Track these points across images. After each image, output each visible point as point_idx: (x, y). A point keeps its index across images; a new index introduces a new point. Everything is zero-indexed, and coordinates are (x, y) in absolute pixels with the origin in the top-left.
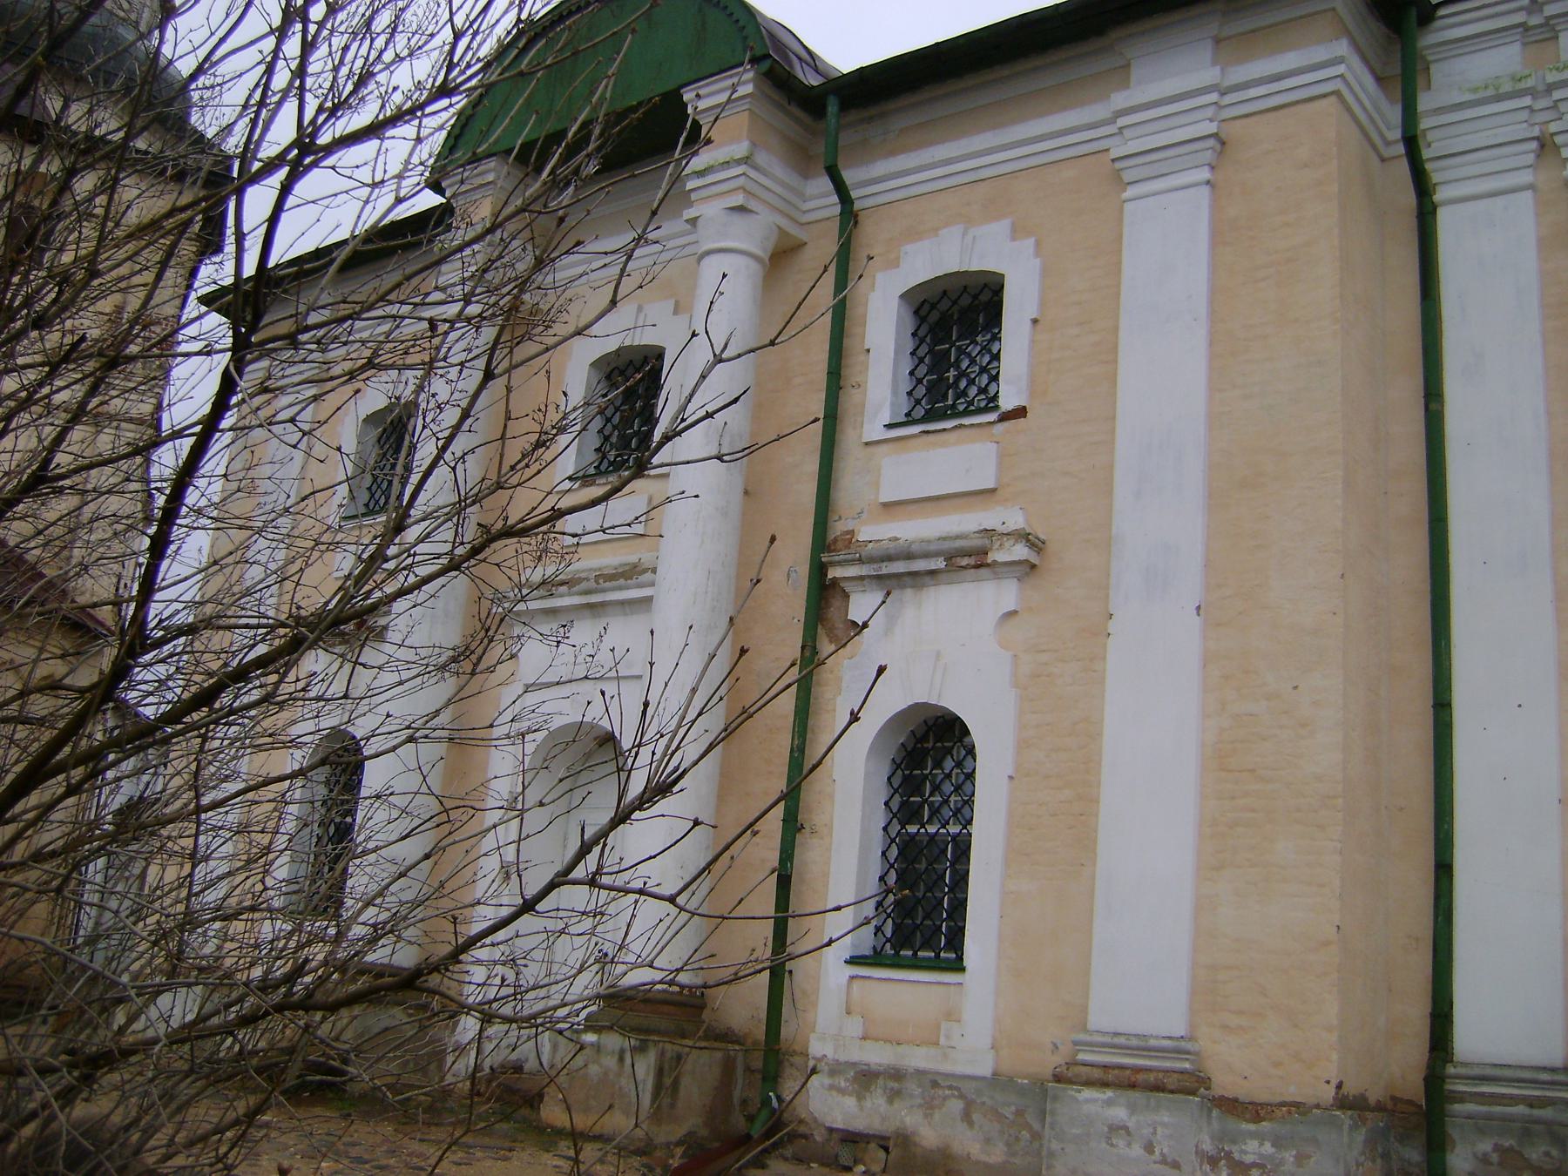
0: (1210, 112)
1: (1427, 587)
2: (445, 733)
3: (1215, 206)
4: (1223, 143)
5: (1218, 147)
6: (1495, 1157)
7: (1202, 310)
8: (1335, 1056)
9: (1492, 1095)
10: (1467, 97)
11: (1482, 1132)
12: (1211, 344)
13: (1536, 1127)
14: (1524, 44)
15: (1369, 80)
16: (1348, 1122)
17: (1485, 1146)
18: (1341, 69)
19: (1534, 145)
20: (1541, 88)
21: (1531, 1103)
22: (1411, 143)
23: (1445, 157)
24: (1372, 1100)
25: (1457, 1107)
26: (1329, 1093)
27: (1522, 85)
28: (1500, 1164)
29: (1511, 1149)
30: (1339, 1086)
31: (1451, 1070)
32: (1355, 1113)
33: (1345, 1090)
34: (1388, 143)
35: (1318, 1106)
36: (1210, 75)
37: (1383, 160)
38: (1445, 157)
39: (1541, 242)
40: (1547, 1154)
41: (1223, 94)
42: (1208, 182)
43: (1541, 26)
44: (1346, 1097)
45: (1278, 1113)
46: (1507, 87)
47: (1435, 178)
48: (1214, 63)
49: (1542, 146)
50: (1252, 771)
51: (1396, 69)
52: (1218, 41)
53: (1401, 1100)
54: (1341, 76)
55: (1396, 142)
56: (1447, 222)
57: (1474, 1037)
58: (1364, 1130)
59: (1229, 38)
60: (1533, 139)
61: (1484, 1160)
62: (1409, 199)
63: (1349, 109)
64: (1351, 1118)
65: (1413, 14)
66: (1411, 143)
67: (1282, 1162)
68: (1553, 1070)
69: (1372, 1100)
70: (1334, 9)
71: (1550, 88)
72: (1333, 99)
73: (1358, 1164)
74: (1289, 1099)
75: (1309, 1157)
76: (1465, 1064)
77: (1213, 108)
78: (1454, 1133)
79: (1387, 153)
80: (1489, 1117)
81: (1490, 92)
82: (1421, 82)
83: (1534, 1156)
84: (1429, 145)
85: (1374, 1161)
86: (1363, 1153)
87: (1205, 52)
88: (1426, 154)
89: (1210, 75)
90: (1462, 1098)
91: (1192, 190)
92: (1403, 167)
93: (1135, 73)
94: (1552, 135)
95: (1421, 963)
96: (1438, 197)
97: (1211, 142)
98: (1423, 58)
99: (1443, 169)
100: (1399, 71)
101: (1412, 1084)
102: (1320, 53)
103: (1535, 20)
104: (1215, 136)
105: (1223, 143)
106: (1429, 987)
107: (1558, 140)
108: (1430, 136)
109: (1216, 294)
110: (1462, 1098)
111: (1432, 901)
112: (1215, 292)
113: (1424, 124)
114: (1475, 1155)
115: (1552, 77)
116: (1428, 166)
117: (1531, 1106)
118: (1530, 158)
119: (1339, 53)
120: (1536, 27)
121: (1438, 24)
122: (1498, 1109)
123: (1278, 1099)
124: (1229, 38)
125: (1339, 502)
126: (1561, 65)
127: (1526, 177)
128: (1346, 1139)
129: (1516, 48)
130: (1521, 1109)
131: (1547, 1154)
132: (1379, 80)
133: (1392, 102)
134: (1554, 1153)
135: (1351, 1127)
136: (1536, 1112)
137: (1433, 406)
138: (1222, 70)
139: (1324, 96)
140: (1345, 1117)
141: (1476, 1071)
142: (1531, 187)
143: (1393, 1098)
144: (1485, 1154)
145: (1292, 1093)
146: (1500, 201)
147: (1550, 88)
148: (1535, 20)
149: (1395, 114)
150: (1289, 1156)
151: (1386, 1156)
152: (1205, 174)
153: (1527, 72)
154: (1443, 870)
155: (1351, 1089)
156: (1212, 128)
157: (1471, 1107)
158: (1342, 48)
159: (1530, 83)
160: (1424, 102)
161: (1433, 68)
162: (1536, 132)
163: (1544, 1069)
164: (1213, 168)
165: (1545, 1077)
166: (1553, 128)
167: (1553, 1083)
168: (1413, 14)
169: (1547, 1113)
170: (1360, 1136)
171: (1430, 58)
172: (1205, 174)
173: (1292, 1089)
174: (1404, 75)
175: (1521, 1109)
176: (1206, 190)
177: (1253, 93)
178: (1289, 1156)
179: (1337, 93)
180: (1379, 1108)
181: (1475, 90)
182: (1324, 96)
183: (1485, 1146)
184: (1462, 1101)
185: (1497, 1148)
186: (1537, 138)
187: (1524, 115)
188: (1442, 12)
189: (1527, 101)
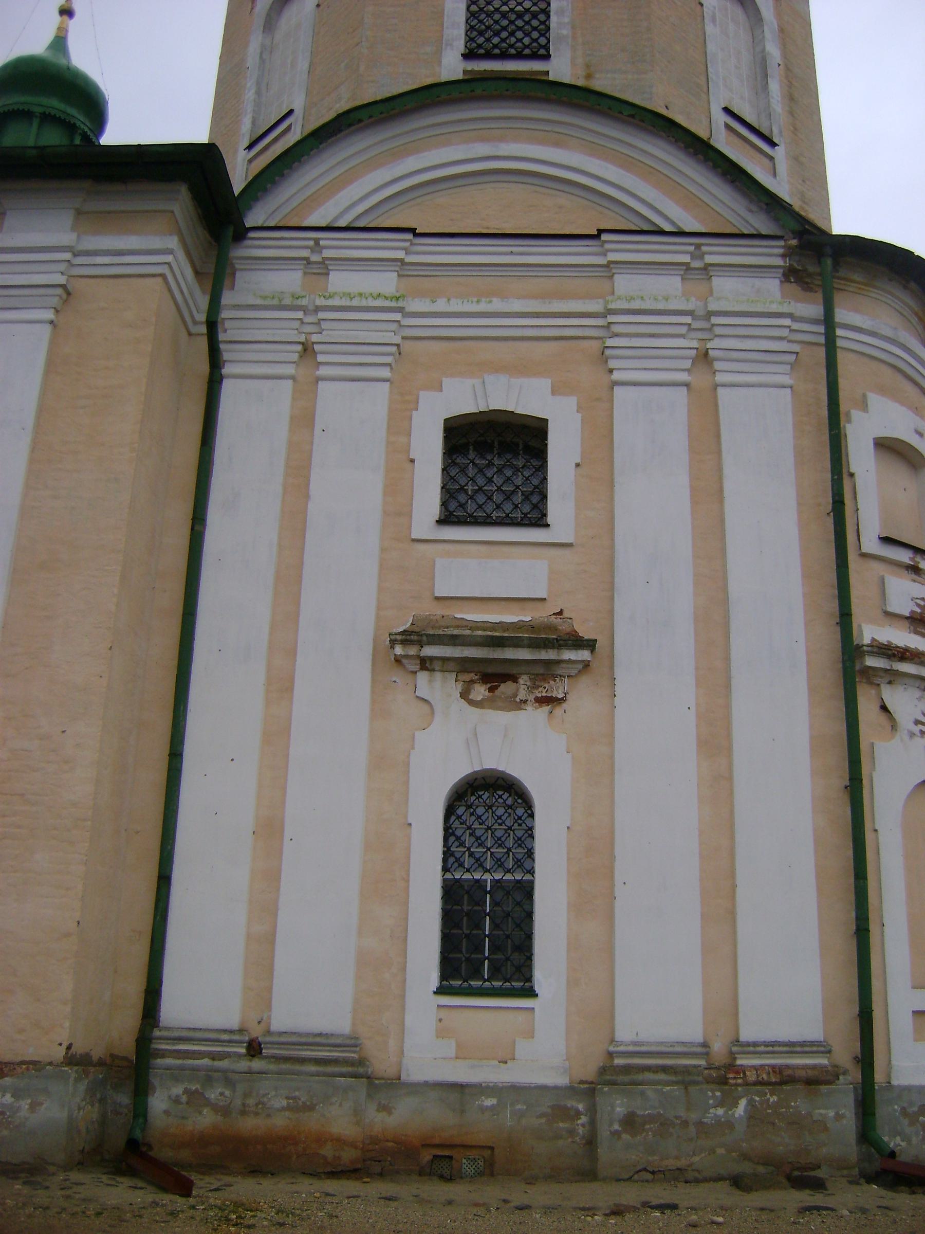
0: (62, 267)
1: (175, 663)
2: (503, 839)
3: (53, 343)
4: (69, 294)
5: (65, 296)
6: (184, 1098)
7: (30, 422)
8: (67, 1024)
9: (187, 1052)
10: (259, 302)
11: (177, 1080)
12: (33, 449)
13: (216, 1074)
14: (305, 273)
15: (189, 272)
16: (73, 1075)
17: (178, 1090)
18: (170, 258)
19: (299, 348)
20: (311, 307)
21: (213, 1056)
22: (212, 326)
23: (256, 342)
24: (95, 1058)
25: (159, 1061)
26: (59, 1053)
27: (299, 302)
28: (187, 1103)
29: (197, 1091)
30: (69, 1047)
31: (157, 1033)
32: (80, 1068)
33: (73, 1050)
34: (195, 323)
35: (50, 1064)
36: (68, 238)
37: (190, 334)
38: (256, 342)
39: (292, 418)
40: (222, 1094)
41: (75, 255)
42: (52, 322)
43: (319, 263)
44: (73, 1056)
45: (19, 1070)
46: (287, 301)
47: (226, 356)
48: (73, 229)
49: (305, 350)
50: (23, 795)
51: (211, 268)
52: (79, 213)
53: (117, 1057)
54: (169, 264)
55: (202, 323)
56: (228, 388)
57: (175, 1009)
58: (86, 1082)
59: (88, 213)
60: (300, 343)
61: (176, 1101)
62: (205, 368)
63: (170, 290)
64: (76, 1072)
65: (230, 231)
66: (212, 326)
67: (19, 1109)
68: (231, 1032)
69: (95, 1058)
70: (172, 212)
71: (318, 309)
72: (160, 280)
73: (79, 1109)
74: (27, 1059)
75: (42, 1104)
76: (168, 1029)
77: (66, 264)
78: (155, 1081)
79: (194, 329)
80: (182, 1068)
81: (275, 302)
82: (227, 282)
83: (213, 1096)
84: (225, 331)
85: (92, 1106)
86: (84, 1099)
87: (67, 218)
88: (222, 337)
89: (68, 238)
90: (163, 1054)
91: (38, 326)
92: (203, 343)
93: (9, 221)
94: (313, 343)
95: (141, 951)
96: (225, 371)
97: (59, 291)
98: (233, 266)
99: (230, 351)
100: (213, 271)
101: (127, 1047)
102: (156, 242)
103: (697, 264)
104: (63, 286)
105: (69, 294)
106: (146, 970)
107: (316, 347)
108: (228, 324)
109: (44, 411)
110: (163, 1054)
111: (153, 906)
112: (42, 410)
113: (224, 314)
114: (170, 1097)
115: (320, 302)
116: (222, 346)
117: (213, 1059)
118: (295, 357)
119: (170, 246)
120: (316, 263)
121: (248, 242)
122: (190, 1062)
123: (19, 1059)
124: (88, 213)
125: (116, 591)
126: (327, 294)
127: (290, 370)
128: (71, 1089)
129: (299, 274)
130: (206, 1061)
131: (222, 1094)
132: (197, 273)
133: (204, 292)
134: (227, 1093)
135: (76, 1080)
136: (217, 1064)
137: (197, 528)
138: (79, 236)
139: (154, 276)
140: (71, 1072)
141: (176, 1034)
142: (293, 378)
143: (112, 1055)
144: (177, 1096)
145: (31, 1053)
146: (269, 383)
147: (318, 309)
148: (697, 264)
149: (204, 302)
150: (25, 1104)
151: (102, 1101)
152: (50, 315)
153: (303, 294)
154: (164, 880)
155: (78, 1049)
156: (62, 280)
157: (169, 1061)
158: (173, 242)
159: (304, 302)
160: (227, 298)
161: (238, 274)
162: (302, 338)
163: (225, 1031)
164: (57, 311)
165: (225, 1037)
166: (314, 338)
167: (230, 1041)
168: (230, 231)
169: (224, 1064)
170: (82, 1087)
171: (237, 266)
172: (50, 315)
173: (31, 1050)
174: (216, 275)
175: (206, 1061)
176: (48, 328)
177: (99, 260)
178: (25, 1104)
179: (163, 276)
180: (101, 1063)
181: (265, 298)
182: (154, 276)
183: (178, 1090)
184: (163, 1056)
185: (186, 1091)
186: (303, 344)
187: (296, 324)
188: (252, 235)
189: (300, 314)
